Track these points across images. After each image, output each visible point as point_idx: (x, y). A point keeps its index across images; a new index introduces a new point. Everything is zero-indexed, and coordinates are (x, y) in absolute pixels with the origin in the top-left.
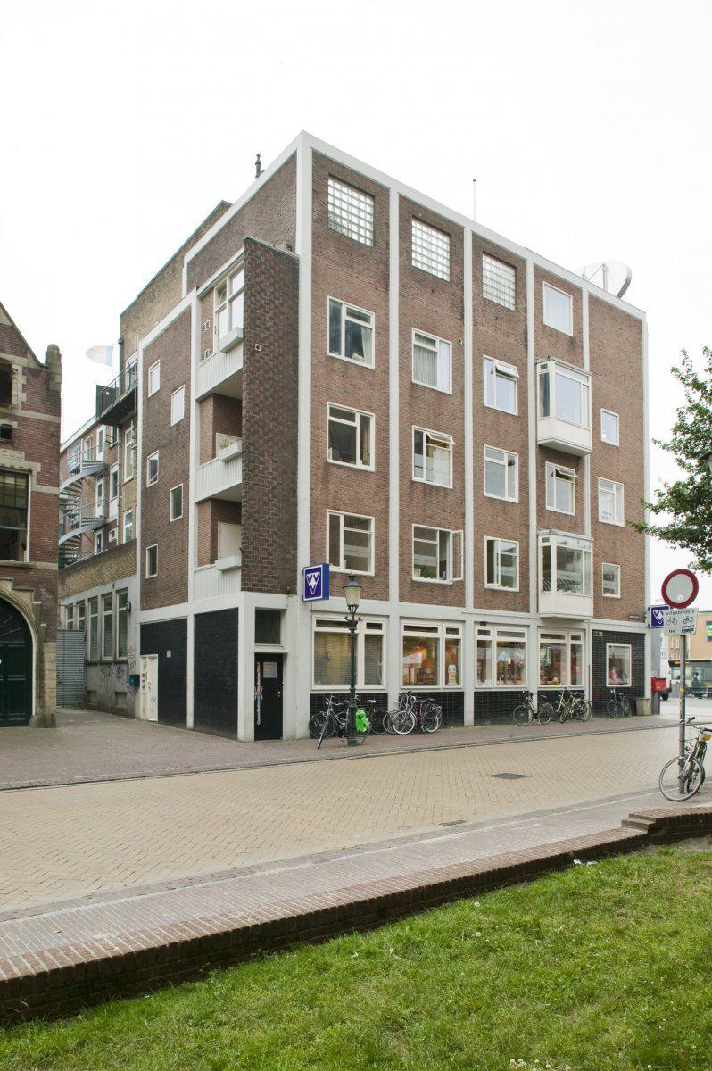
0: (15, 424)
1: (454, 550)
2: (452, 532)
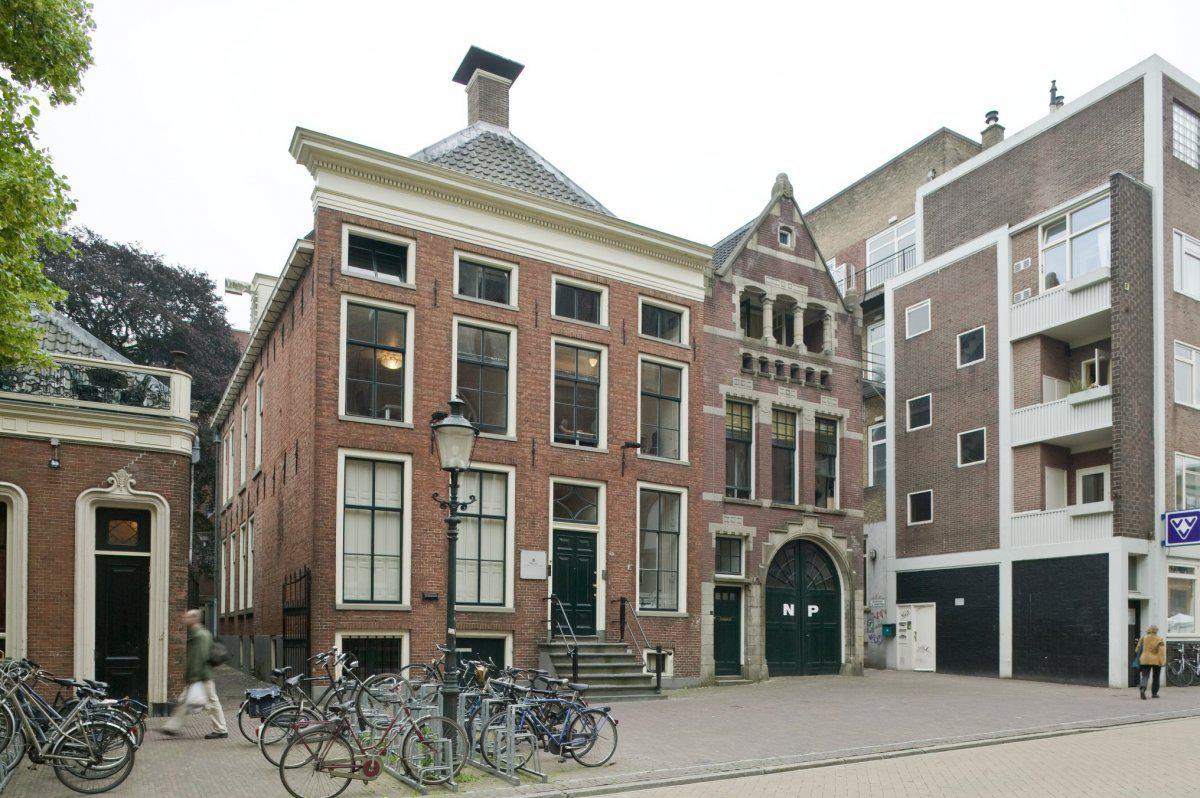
0: (830, 371)
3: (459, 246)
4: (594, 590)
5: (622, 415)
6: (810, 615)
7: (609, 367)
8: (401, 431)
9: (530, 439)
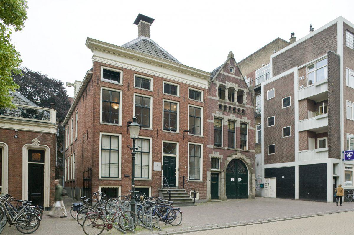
0: (245, 109)
1: (68, 163)
2: (163, 155)
3: (135, 72)
4: (175, 174)
5: (183, 122)
6: (239, 181)
7: (180, 108)
8: (118, 127)
9: (156, 129)
